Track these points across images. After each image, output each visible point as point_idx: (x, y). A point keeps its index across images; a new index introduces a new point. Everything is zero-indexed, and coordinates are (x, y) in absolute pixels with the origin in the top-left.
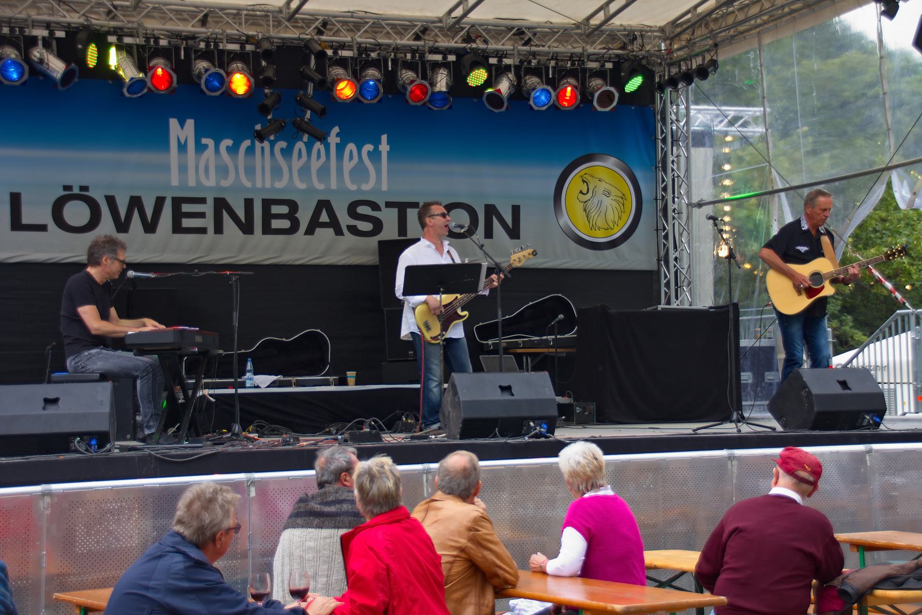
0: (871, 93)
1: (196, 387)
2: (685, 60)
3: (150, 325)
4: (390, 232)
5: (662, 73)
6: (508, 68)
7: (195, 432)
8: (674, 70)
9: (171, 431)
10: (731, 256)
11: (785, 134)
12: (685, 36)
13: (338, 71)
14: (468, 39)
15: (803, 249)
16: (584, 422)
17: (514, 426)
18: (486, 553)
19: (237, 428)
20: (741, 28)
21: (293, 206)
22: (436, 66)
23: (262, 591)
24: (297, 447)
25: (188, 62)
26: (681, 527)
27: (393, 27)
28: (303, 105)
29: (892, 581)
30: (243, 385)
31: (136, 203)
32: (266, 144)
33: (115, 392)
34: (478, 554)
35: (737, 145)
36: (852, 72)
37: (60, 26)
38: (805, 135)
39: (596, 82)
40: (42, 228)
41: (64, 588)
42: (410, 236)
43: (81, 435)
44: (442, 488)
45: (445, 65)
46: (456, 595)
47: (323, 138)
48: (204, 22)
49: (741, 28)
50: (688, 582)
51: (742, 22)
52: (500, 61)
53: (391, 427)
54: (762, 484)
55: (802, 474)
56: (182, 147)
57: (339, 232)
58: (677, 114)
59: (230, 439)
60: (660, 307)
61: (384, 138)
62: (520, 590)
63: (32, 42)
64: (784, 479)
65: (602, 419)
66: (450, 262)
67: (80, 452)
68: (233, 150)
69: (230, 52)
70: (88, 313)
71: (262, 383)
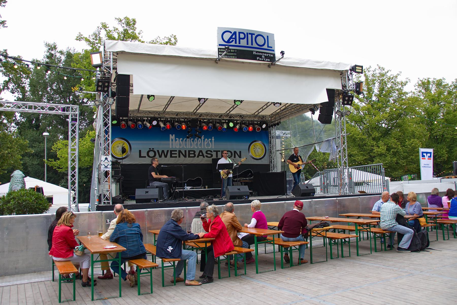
0: (311, 129)
1: (175, 189)
2: (274, 121)
3: (165, 177)
4: (214, 157)
5: (270, 124)
6: (238, 123)
7: (175, 198)
8: (272, 124)
9: (170, 198)
10: (284, 161)
11: (295, 136)
12: (274, 117)
13: (204, 124)
14: (230, 117)
15: (295, 159)
16: (255, 196)
17: (240, 197)
18: (235, 223)
19: (183, 198)
20: (285, 115)
21: (194, 152)
22: (224, 123)
23: (190, 231)
24: (196, 201)
25: (174, 123)
26: (275, 217)
27: (215, 115)
28: (197, 131)
29: (316, 226)
30: (184, 189)
31: (163, 151)
32: (189, 139)
33: (159, 190)
34: (234, 223)
35: (285, 139)
36: (307, 124)
37: (149, 117)
38: (299, 137)
39: (256, 126)
40: (145, 157)
41: (151, 230)
42: (218, 157)
43: (153, 199)
44: (226, 210)
45: (225, 122)
46: (229, 232)
47: (200, 138)
48: (177, 115)
49: (285, 115)
50: (276, 228)
51: (285, 114)
52: (237, 122)
53: (215, 197)
54: (291, 208)
55: (299, 206)
56: (172, 140)
57: (204, 157)
58: (273, 132)
59: (182, 200)
60: (270, 172)
61: (213, 137)
62: (242, 231)
63: (144, 120)
64: (295, 207)
65: (259, 195)
66: (229, 163)
67: (153, 202)
68: (182, 141)
69: (182, 121)
70: (153, 174)
71: (188, 188)
